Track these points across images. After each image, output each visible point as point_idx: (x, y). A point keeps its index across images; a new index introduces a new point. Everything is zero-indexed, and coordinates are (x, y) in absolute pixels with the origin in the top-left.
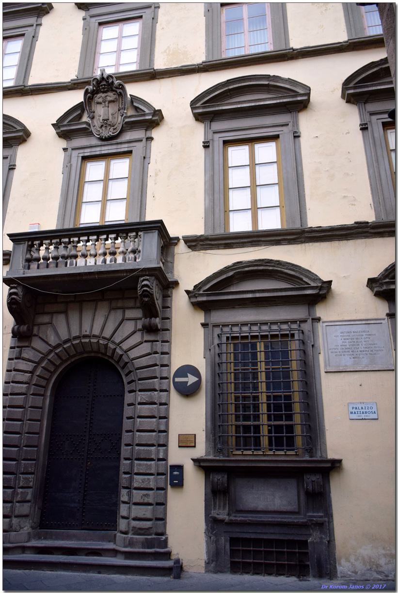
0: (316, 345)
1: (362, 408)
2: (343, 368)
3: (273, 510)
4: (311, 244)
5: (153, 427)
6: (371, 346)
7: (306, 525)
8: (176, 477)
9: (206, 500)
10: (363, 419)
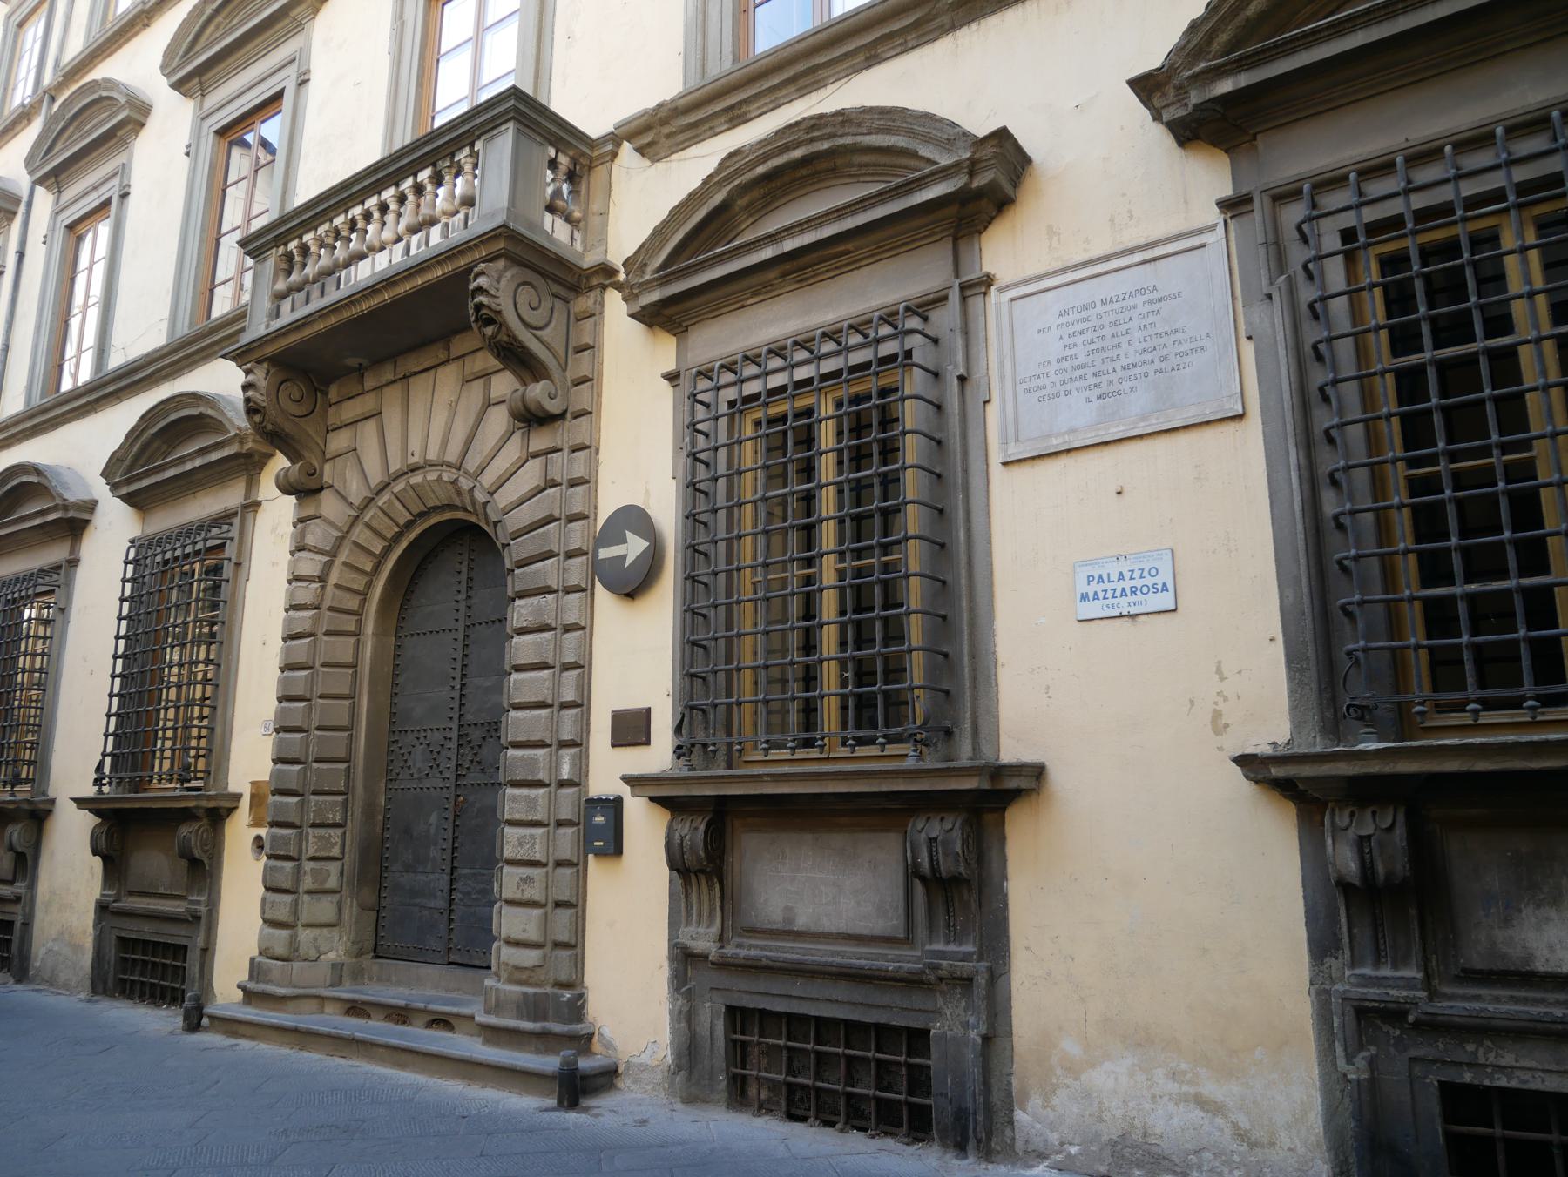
0: (977, 375)
1: (1121, 577)
2: (1060, 440)
3: (834, 930)
4: (974, 26)
5: (545, 695)
6: (1161, 341)
7: (922, 982)
8: (602, 830)
9: (671, 895)
10: (1121, 616)
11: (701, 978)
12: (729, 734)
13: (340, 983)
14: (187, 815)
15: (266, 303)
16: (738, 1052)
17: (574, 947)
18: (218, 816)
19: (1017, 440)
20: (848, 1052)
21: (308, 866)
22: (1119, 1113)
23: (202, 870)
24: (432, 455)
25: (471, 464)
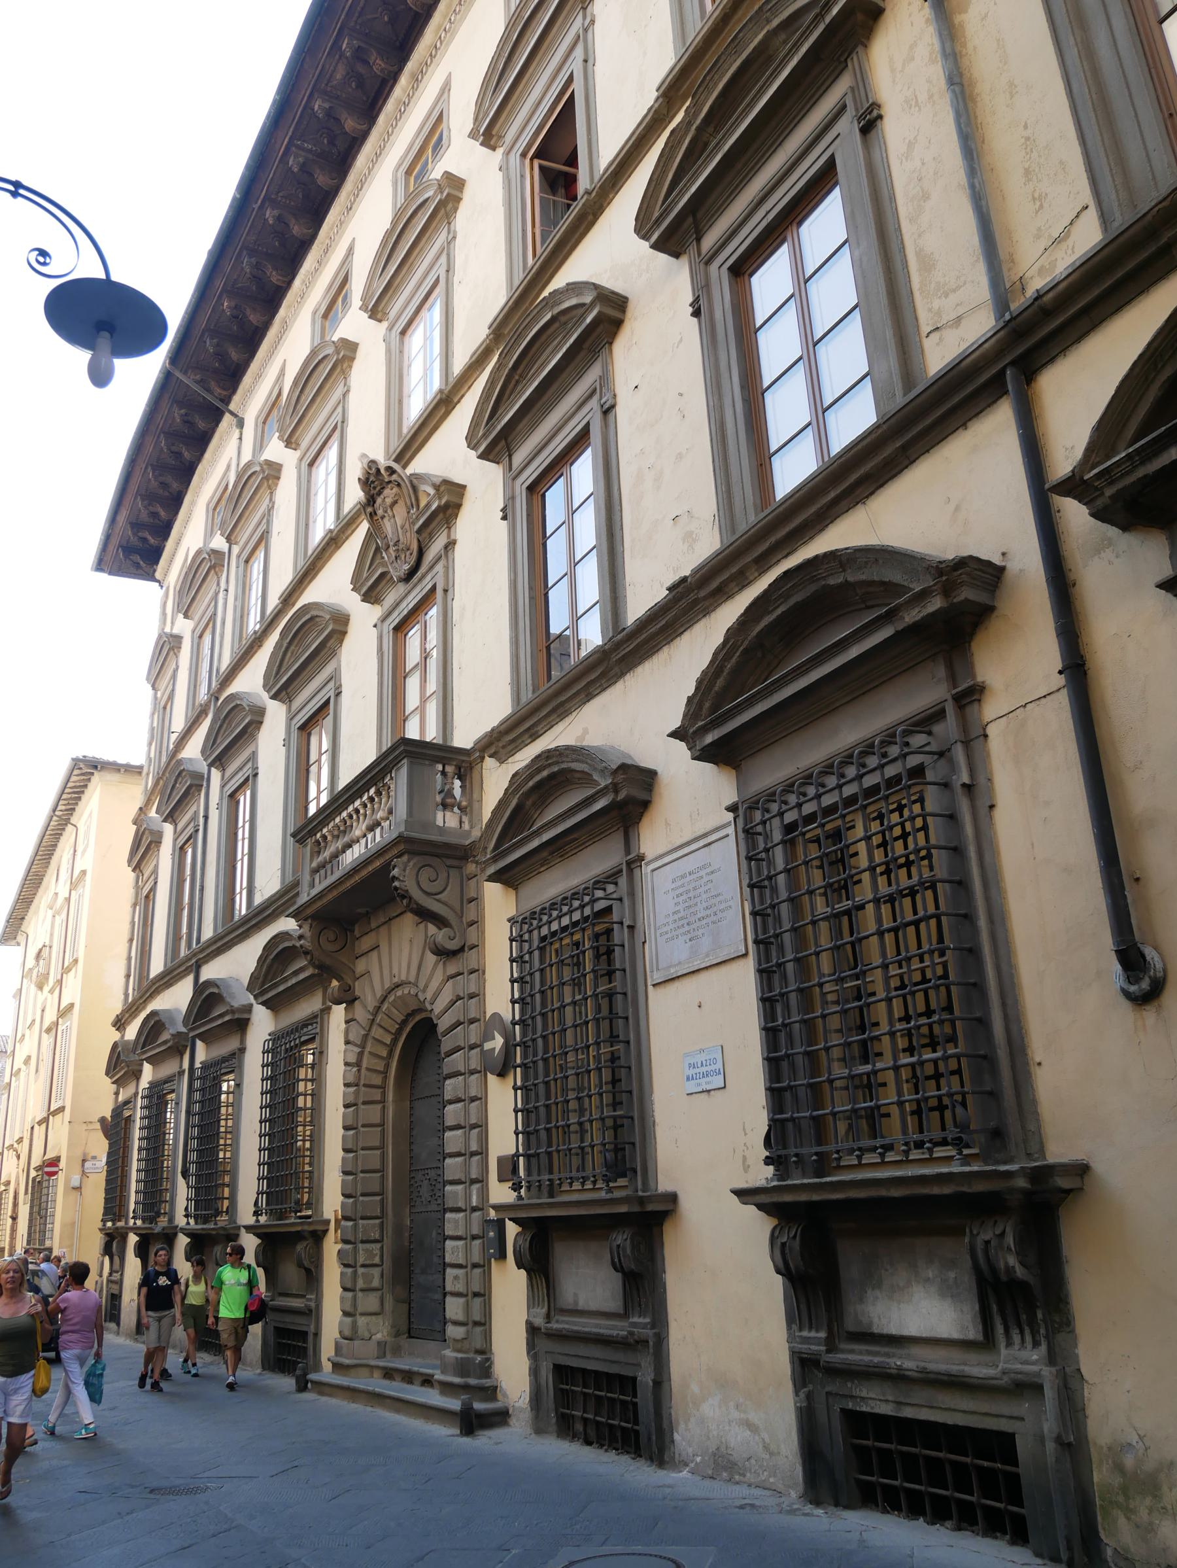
0: (639, 925)
11: (543, 1344)
12: (551, 1172)
13: (384, 1355)
14: (298, 1236)
15: (307, 878)
16: (564, 1398)
17: (484, 1324)
18: (318, 1237)
19: (658, 969)
20: (609, 1395)
21: (361, 1270)
22: (715, 1433)
23: (312, 1276)
24: (403, 978)
25: (421, 985)
